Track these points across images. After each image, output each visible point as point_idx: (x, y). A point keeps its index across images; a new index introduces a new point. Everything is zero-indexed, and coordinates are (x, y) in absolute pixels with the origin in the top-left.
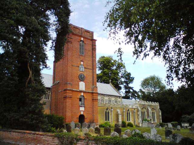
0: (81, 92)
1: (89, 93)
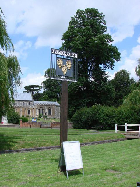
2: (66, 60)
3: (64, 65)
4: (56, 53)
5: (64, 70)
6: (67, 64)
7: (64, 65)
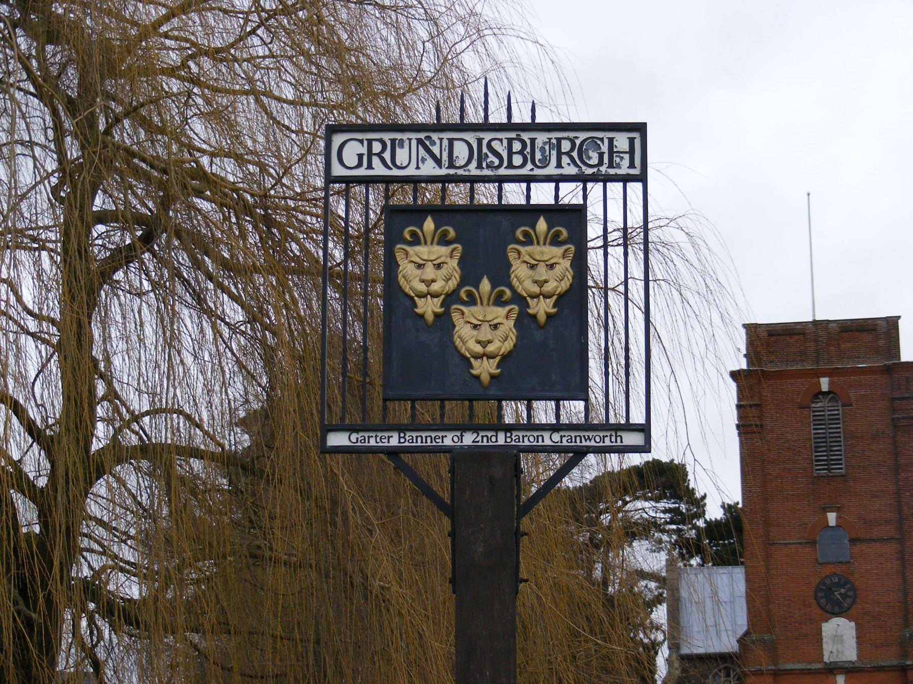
0: (833, 669)
1: (880, 669)
2: (505, 221)
3: (485, 285)
4: (379, 170)
5: (485, 333)
6: (520, 273)
7: (485, 285)
